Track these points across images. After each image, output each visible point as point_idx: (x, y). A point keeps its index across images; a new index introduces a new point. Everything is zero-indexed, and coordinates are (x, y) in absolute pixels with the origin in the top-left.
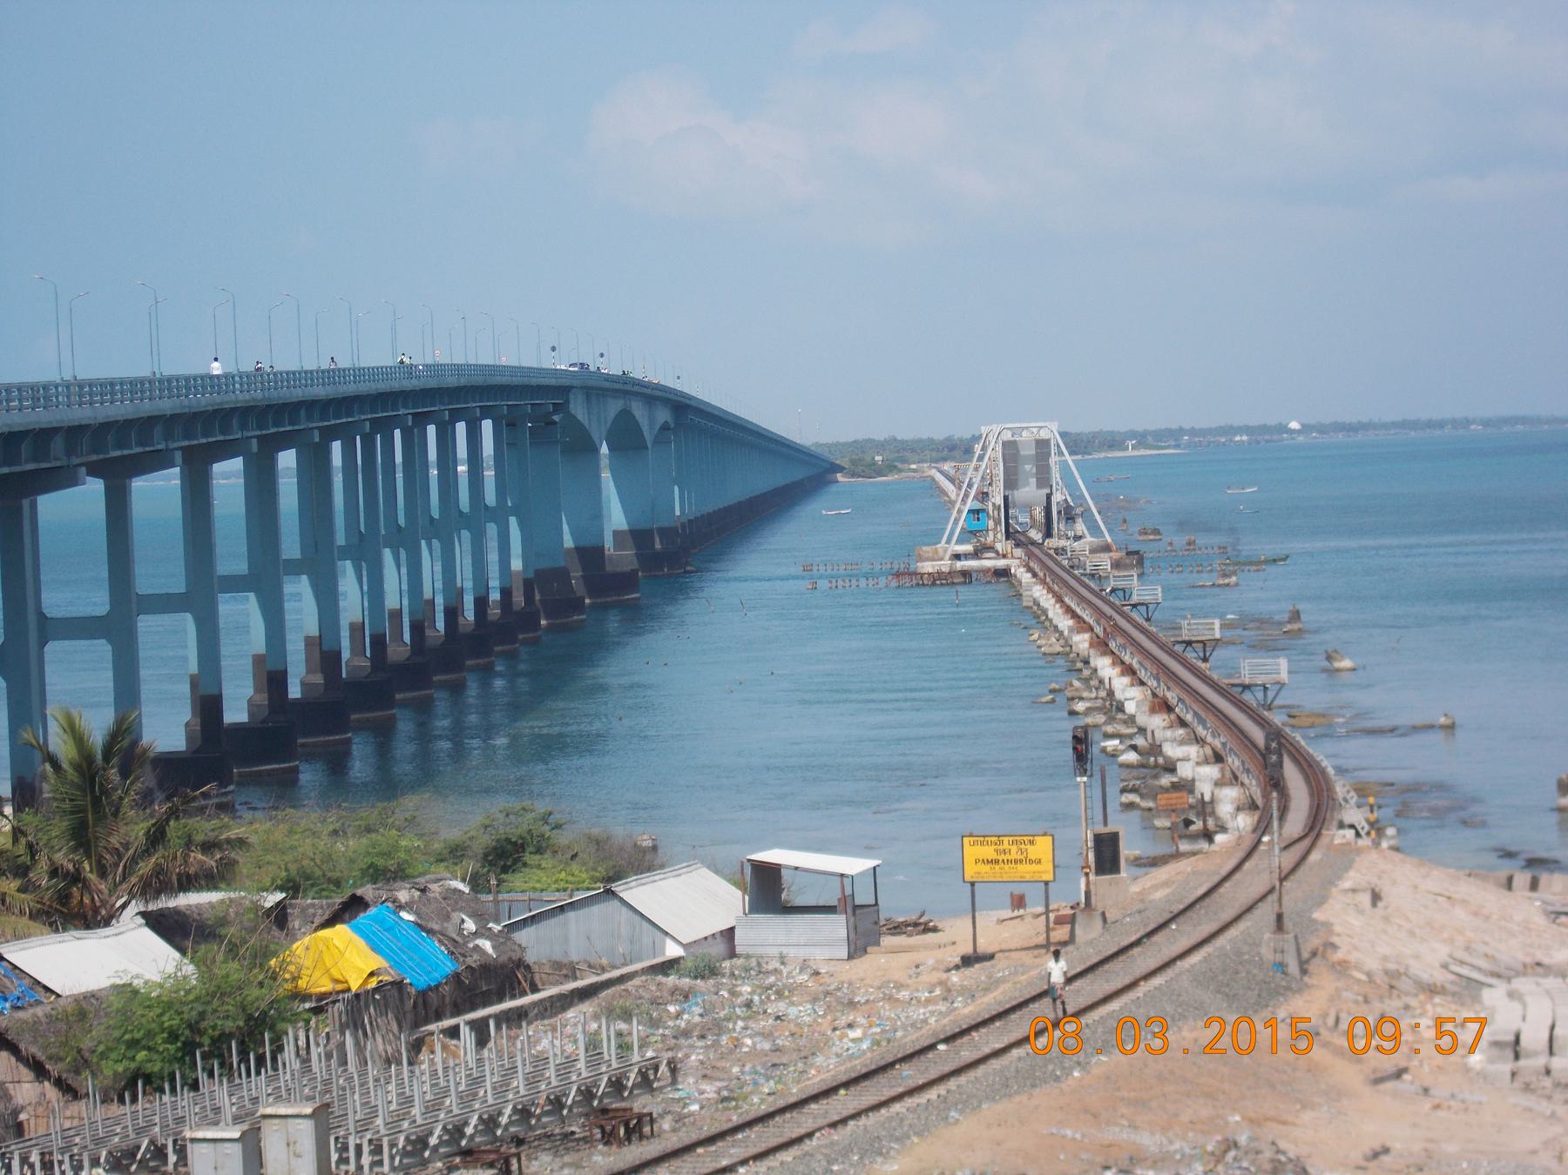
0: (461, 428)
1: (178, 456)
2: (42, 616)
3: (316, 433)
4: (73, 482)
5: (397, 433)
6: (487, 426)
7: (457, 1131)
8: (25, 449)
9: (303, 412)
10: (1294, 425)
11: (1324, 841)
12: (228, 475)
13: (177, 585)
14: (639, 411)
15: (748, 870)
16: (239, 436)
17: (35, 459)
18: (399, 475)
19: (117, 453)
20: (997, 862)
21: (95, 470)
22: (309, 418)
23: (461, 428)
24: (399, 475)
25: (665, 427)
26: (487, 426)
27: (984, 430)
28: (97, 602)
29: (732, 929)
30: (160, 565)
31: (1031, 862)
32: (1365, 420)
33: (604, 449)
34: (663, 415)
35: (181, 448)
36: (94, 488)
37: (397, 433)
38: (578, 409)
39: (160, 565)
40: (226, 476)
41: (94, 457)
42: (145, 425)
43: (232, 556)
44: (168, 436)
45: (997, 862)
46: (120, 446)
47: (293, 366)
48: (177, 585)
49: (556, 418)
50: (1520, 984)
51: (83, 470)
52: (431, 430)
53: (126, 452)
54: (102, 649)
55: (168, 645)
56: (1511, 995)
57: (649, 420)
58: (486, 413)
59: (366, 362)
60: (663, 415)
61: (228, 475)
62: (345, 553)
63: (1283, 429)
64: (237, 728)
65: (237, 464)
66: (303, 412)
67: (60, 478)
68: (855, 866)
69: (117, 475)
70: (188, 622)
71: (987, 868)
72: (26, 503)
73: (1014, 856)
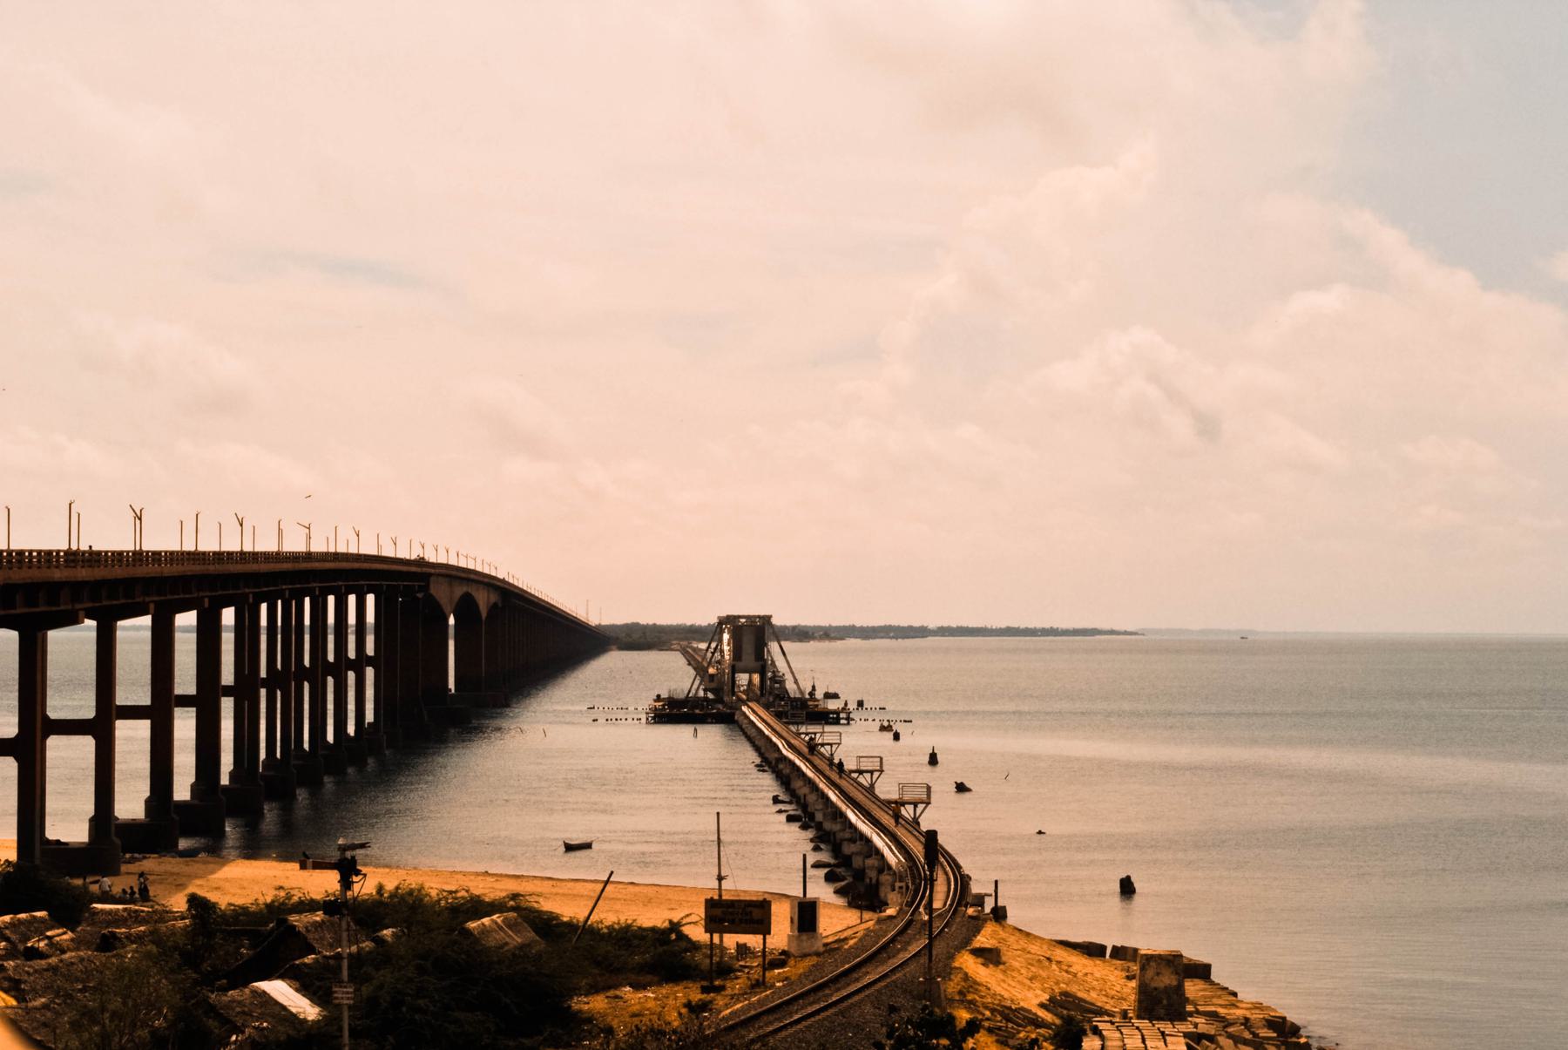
1: (152, 606)
6: (370, 599)
12: (135, 632)
13: (144, 699)
23: (331, 599)
26: (370, 599)
33: (452, 621)
35: (255, 594)
42: (129, 584)
43: (185, 680)
49: (420, 595)
51: (82, 613)
57: (483, 600)
60: (494, 598)
67: (71, 619)
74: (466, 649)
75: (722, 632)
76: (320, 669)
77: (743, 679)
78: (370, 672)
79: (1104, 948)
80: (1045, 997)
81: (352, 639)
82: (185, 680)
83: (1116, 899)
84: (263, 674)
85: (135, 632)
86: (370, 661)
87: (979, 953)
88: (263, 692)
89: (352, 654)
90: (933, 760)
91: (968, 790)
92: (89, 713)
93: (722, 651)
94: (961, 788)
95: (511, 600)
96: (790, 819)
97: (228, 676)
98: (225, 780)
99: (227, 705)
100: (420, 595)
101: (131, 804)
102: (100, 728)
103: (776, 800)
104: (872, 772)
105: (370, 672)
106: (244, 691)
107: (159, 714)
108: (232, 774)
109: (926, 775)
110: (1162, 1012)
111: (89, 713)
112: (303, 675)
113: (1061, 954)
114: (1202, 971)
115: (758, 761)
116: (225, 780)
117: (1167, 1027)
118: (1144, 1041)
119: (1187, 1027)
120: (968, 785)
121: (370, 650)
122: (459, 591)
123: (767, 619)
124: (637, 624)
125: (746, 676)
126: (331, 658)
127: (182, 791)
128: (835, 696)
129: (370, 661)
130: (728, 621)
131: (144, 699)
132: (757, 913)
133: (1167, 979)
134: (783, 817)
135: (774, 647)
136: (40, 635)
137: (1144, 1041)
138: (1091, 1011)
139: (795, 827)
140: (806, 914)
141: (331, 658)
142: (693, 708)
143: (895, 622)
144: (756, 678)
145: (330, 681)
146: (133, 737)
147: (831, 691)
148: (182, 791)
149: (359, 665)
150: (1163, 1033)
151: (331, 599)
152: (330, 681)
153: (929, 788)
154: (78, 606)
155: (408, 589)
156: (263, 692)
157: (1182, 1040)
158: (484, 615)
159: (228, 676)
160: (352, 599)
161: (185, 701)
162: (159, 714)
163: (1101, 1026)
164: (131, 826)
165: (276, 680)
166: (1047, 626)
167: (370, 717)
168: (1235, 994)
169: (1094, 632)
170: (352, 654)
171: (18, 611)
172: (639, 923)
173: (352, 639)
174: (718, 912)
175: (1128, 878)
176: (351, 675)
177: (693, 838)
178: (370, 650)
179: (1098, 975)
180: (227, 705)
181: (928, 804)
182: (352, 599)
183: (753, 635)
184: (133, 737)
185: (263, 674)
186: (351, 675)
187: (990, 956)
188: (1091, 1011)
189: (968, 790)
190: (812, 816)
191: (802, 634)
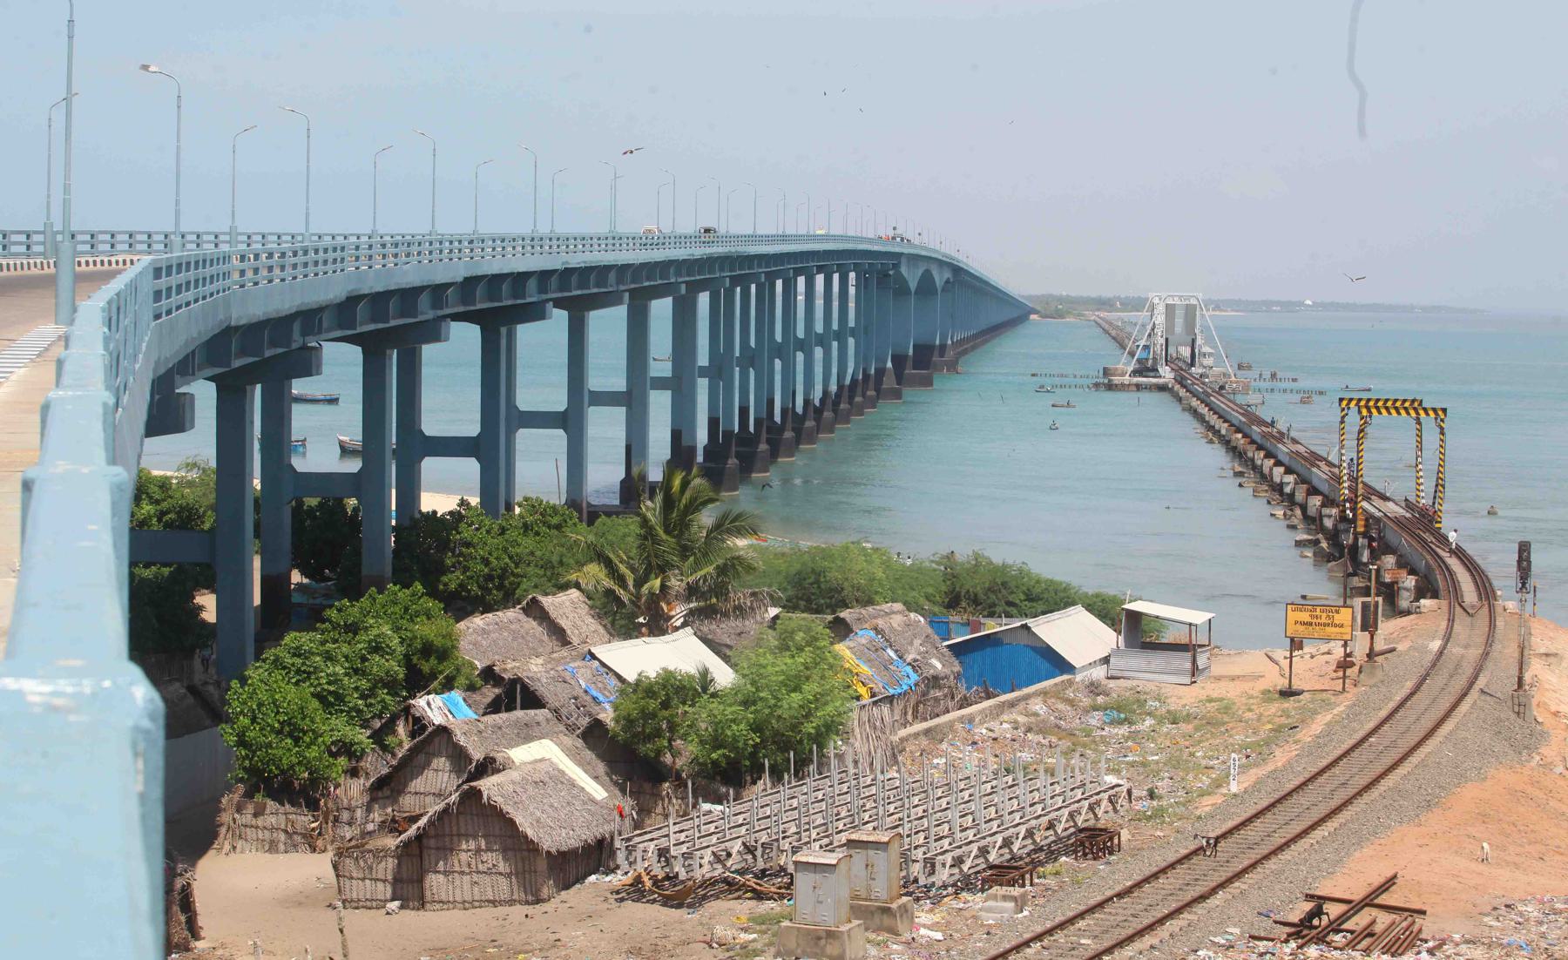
0: (801, 281)
1: (627, 295)
3: (683, 287)
5: (753, 287)
6: (852, 275)
8: (574, 279)
9: (672, 271)
10: (1308, 302)
12: (661, 310)
14: (935, 274)
17: (598, 286)
21: (559, 304)
22: (760, 266)
23: (801, 281)
25: (947, 282)
26: (852, 275)
27: (1151, 295)
28: (557, 401)
30: (607, 371)
34: (947, 275)
35: (686, 282)
36: (560, 317)
37: (753, 287)
38: (904, 270)
39: (607, 371)
42: (601, 272)
43: (660, 363)
44: (679, 274)
46: (648, 279)
52: (779, 283)
53: (381, 326)
55: (606, 429)
57: (940, 277)
58: (820, 269)
60: (947, 275)
61: (661, 310)
62: (703, 372)
63: (1301, 304)
65: (667, 303)
67: (534, 313)
68: (1199, 617)
69: (578, 309)
70: (620, 412)
71: (1302, 628)
72: (504, 330)
73: (1323, 620)
74: (915, 321)
82: (660, 363)
86: (853, 332)
89: (801, 334)
92: (472, 428)
95: (962, 280)
97: (703, 359)
99: (703, 384)
105: (851, 341)
106: (718, 371)
107: (679, 384)
108: (20, 694)
112: (822, 341)
124: (1051, 295)
126: (779, 338)
129: (853, 332)
131: (619, 383)
141: (779, 338)
146: (660, 405)
149: (840, 336)
154: (622, 288)
155: (881, 273)
159: (703, 359)
161: (660, 384)
162: (632, 400)
165: (750, 359)
170: (801, 334)
172: (1085, 589)
177: (438, 906)
180: (703, 384)
182: (820, 279)
184: (660, 405)
186: (800, 356)
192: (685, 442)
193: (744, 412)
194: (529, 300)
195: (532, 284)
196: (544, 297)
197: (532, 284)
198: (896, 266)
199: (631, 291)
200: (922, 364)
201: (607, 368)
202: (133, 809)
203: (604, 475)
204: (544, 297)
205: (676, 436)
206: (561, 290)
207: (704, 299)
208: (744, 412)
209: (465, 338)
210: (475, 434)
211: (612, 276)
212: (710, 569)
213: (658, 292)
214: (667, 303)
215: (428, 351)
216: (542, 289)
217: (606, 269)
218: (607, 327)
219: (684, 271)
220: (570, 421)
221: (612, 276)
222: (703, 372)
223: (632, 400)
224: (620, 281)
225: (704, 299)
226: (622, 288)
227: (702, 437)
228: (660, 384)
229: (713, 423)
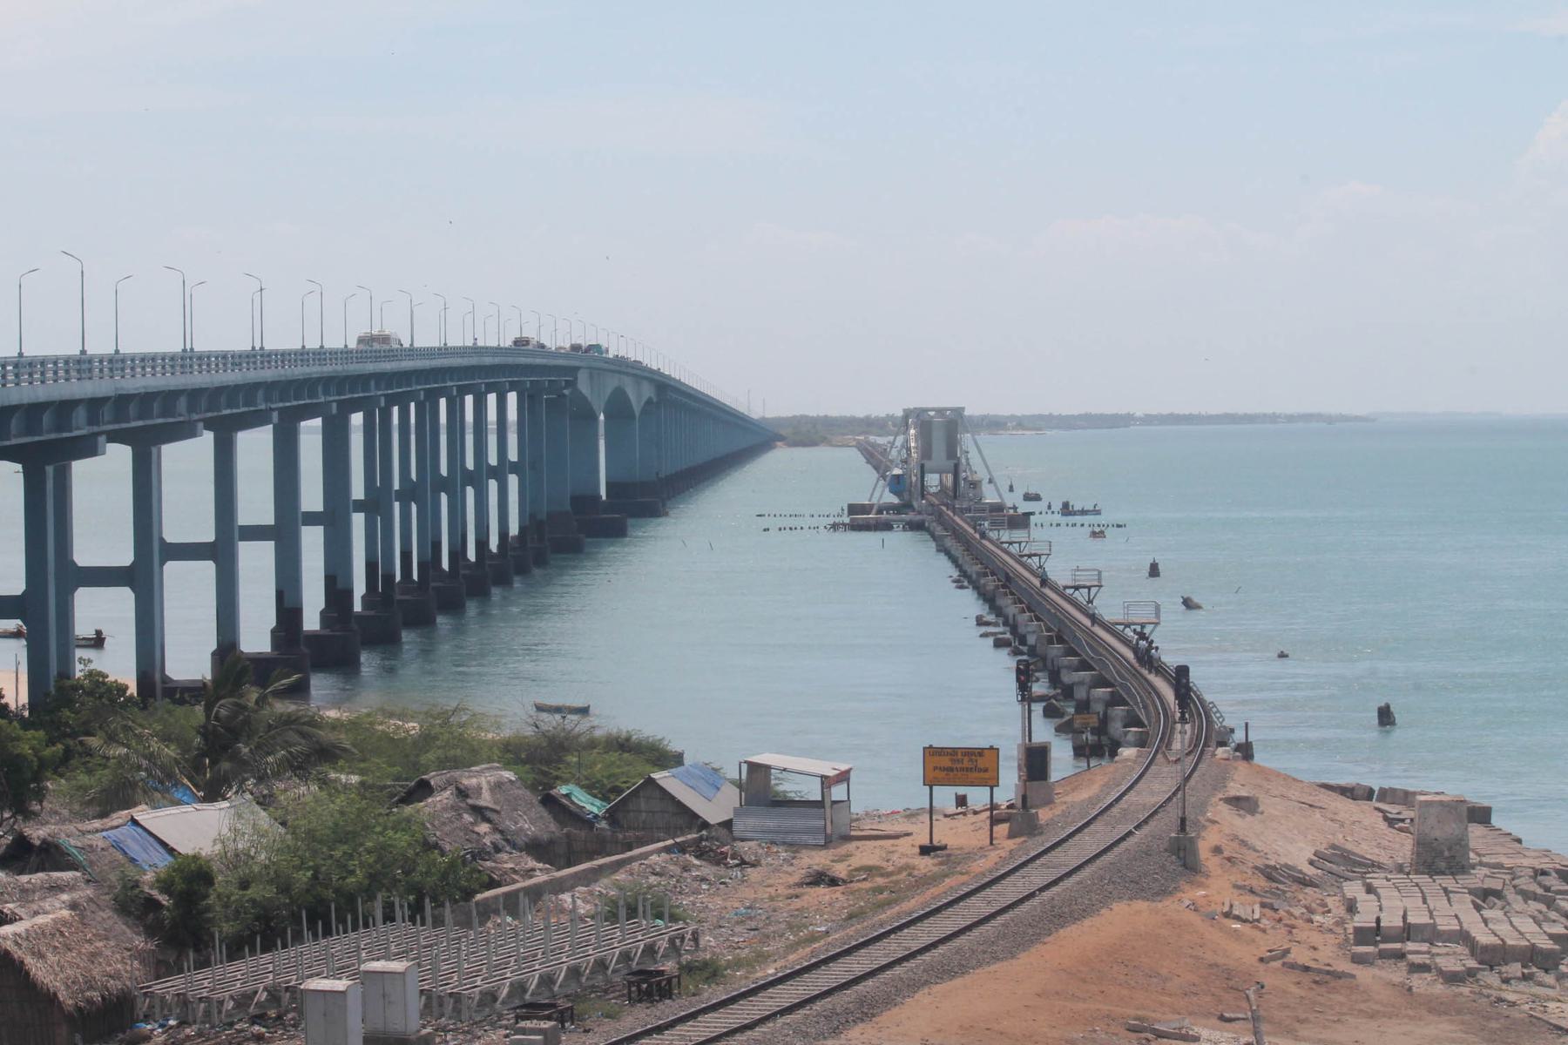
1: (275, 415)
2: (162, 540)
3: (334, 405)
4: (192, 434)
6: (512, 398)
7: (519, 988)
8: (132, 409)
9: (373, 383)
11: (1207, 756)
12: (311, 433)
13: (268, 519)
15: (745, 767)
16: (322, 400)
18: (413, 437)
19: (228, 412)
20: (951, 770)
21: (114, 437)
22: (378, 388)
23: (469, 399)
24: (413, 437)
25: (649, 402)
26: (512, 398)
29: (730, 821)
31: (980, 770)
32: (1195, 412)
33: (602, 417)
35: (386, 396)
36: (208, 438)
38: (583, 386)
40: (311, 431)
41: (209, 415)
42: (249, 390)
43: (312, 497)
45: (951, 770)
46: (229, 406)
47: (292, 343)
48: (268, 519)
49: (566, 392)
50: (1377, 880)
51: (201, 425)
54: (207, 569)
55: (188, 591)
56: (1370, 889)
57: (638, 396)
59: (132, 345)
60: (648, 392)
62: (359, 506)
64: (313, 637)
65: (317, 422)
66: (373, 383)
67: (88, 448)
72: (50, 470)
74: (607, 454)
75: (907, 427)
76: (476, 480)
77: (932, 480)
78: (513, 481)
79: (1371, 791)
80: (1309, 854)
81: (492, 440)
82: (312, 497)
83: (1373, 733)
84: (396, 486)
85: (255, 448)
86: (515, 468)
87: (1236, 802)
88: (397, 505)
89: (493, 460)
90: (1154, 571)
91: (1198, 607)
92: (207, 535)
93: (908, 449)
94: (1188, 604)
95: (672, 400)
96: (999, 644)
97: (358, 491)
98: (358, 607)
99: (358, 520)
100: (566, 392)
101: (256, 637)
102: (219, 555)
103: (980, 622)
104: (1089, 588)
105: (513, 481)
106: (375, 505)
107: (283, 533)
109: (1149, 591)
110: (1443, 865)
111: (207, 535)
113: (1326, 798)
114: (1481, 815)
115: (956, 574)
116: (358, 607)
117: (1448, 882)
118: (1425, 902)
119: (1465, 881)
120: (1196, 599)
121: (513, 456)
122: (611, 383)
123: (959, 411)
125: (937, 476)
126: (444, 471)
127: (311, 621)
128: (1037, 498)
129: (515, 468)
130: (908, 414)
132: (981, 763)
133: (1448, 830)
134: (991, 641)
135: (966, 440)
136: (154, 450)
137: (1425, 902)
138: (1360, 864)
139: (1004, 653)
140: (1035, 762)
141: (444, 471)
142: (880, 512)
143: (1095, 410)
144: (950, 477)
145: (470, 491)
146: (257, 561)
147: (1032, 491)
148: (311, 621)
149: (499, 473)
150: (1445, 890)
151: (469, 399)
152: (470, 491)
153: (1158, 608)
154: (195, 417)
155: (553, 388)
156: (397, 505)
157: (1469, 898)
158: (637, 410)
159: (358, 491)
160: (492, 399)
161: (312, 519)
162: (283, 533)
163: (1376, 883)
164: (258, 661)
165: (409, 493)
166: (1165, 411)
167: (514, 530)
168: (1519, 841)
169: (1125, 420)
170: (493, 460)
171: (14, 442)
173: (492, 440)
174: (946, 762)
175: (1388, 707)
176: (493, 485)
178: (513, 456)
179: (1366, 822)
180: (358, 520)
181: (1157, 624)
182: (492, 399)
183: (942, 432)
184: (257, 561)
185: (396, 486)
186: (493, 485)
187: (1242, 804)
188: (1360, 864)
189: (1198, 607)
190: (1023, 641)
191: (994, 424)
192: (340, 585)
193: (406, 556)
194: (76, 433)
195: (80, 415)
196: (96, 429)
197: (80, 415)
198: (571, 384)
199: (281, 411)
200: (641, 500)
201: (187, 513)
202: (798, 412)
203: (189, 657)
204: (96, 429)
205: (330, 581)
206: (116, 421)
207: (357, 419)
208: (406, 556)
209: (118, 457)
210: (19, 593)
211: (182, 404)
212: (355, 779)
213: (308, 412)
214: (317, 422)
215: (79, 468)
216: (93, 420)
217: (256, 386)
218: (187, 463)
219: (204, 404)
220: (140, 578)
221: (182, 404)
222: (359, 506)
223: (219, 555)
224: (192, 408)
225: (357, 419)
226: (195, 417)
227: (359, 588)
228: (312, 519)
229: (371, 567)
